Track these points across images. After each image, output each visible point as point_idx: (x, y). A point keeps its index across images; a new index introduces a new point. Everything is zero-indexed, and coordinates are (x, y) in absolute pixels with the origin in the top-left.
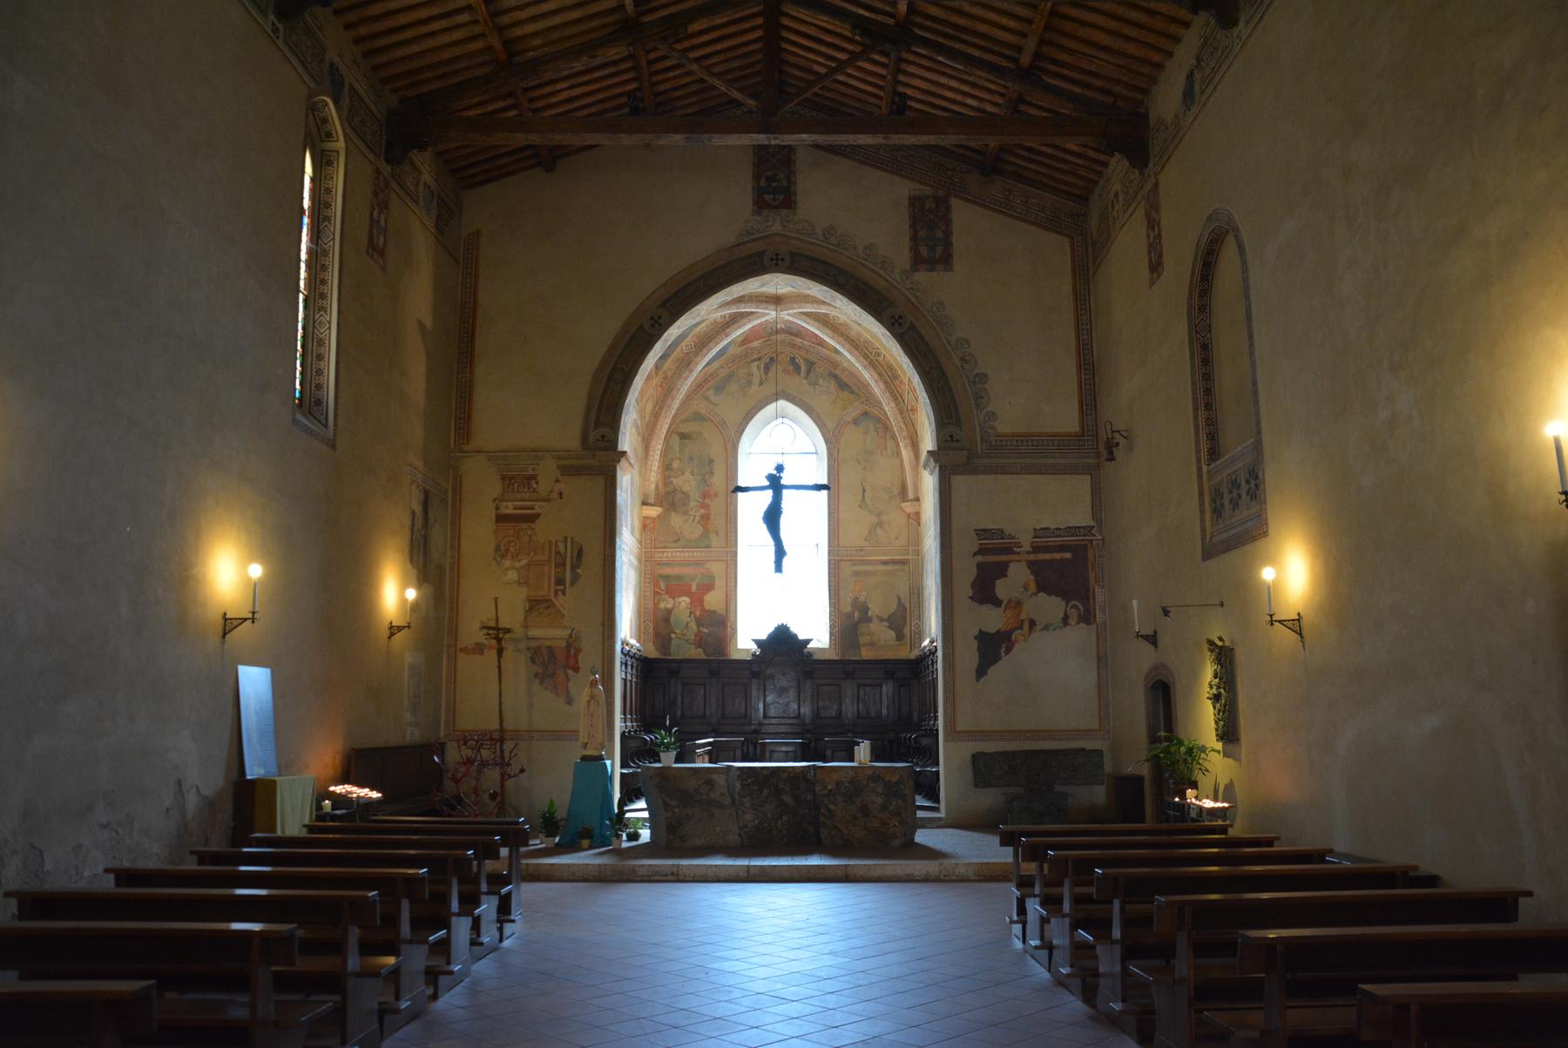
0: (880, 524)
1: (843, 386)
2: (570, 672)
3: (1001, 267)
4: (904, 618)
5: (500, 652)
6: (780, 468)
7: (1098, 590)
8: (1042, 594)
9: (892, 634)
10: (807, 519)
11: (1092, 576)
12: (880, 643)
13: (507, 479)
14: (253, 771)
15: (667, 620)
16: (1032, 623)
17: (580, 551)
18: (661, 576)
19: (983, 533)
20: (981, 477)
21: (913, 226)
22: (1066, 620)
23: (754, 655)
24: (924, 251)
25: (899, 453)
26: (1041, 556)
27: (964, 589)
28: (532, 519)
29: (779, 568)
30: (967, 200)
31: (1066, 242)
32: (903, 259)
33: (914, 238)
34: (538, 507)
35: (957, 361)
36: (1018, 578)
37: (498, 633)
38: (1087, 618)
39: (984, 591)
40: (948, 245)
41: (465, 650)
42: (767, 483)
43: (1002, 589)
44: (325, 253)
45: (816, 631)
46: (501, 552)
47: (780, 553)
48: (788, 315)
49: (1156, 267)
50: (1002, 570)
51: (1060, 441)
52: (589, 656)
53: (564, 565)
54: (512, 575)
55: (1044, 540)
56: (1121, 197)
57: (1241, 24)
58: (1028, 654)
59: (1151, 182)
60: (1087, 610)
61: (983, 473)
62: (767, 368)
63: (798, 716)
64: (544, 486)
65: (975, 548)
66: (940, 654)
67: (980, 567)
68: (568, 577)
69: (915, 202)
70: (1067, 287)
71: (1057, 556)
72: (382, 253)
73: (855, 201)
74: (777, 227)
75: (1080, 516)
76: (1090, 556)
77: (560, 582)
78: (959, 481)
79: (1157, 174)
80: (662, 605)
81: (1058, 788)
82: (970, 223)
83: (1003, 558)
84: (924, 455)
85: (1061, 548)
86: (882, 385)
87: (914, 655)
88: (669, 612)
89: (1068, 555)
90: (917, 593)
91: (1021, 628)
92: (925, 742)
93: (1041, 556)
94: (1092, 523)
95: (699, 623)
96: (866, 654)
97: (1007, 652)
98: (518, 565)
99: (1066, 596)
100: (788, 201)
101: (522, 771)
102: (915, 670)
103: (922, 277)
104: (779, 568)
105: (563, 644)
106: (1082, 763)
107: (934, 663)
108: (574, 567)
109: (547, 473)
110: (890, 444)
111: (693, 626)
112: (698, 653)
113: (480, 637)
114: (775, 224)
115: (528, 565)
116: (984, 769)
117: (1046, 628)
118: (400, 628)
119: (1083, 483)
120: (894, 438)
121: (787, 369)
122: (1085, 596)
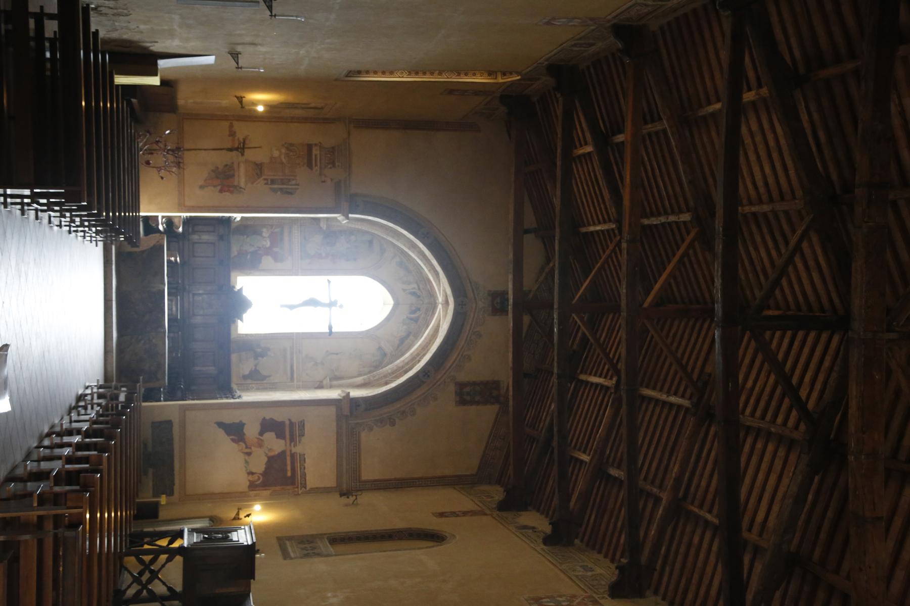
0: (316, 364)
1: (402, 341)
2: (219, 188)
4: (257, 379)
5: (231, 150)
6: (341, 306)
7: (268, 492)
8: (266, 459)
9: (247, 372)
10: (311, 322)
11: (278, 488)
12: (241, 366)
13: (333, 150)
14: (162, 63)
16: (249, 454)
17: (290, 193)
19: (302, 425)
20: (335, 424)
21: (482, 383)
22: (251, 473)
23: (234, 287)
24: (467, 389)
25: (360, 375)
26: (288, 458)
27: (269, 414)
28: (310, 165)
29: (282, 306)
30: (497, 415)
32: (463, 377)
33: (475, 384)
36: (276, 445)
37: (241, 148)
38: (252, 486)
39: (268, 426)
40: (472, 403)
41: (231, 126)
42: (333, 300)
43: (270, 436)
45: (247, 326)
46: (290, 147)
47: (292, 307)
49: (442, 515)
50: (280, 435)
51: (356, 470)
52: (228, 198)
53: (283, 184)
54: (276, 153)
55: (297, 460)
56: (589, 574)
57: (544, 547)
58: (226, 447)
59: (488, 512)
60: (257, 486)
61: (337, 424)
62: (413, 294)
63: (194, 315)
65: (293, 420)
66: (232, 401)
67: (282, 425)
68: (276, 186)
69: (496, 384)
70: (447, 472)
71: (289, 468)
72: (548, 23)
73: (493, 359)
75: (312, 481)
76: (288, 487)
77: (273, 182)
78: (333, 410)
79: (492, 515)
81: (151, 471)
82: (484, 416)
83: (288, 436)
84: (348, 391)
85: (293, 470)
86: (401, 365)
87: (234, 386)
88: (260, 234)
89: (289, 474)
90: (274, 387)
91: (247, 447)
92: (179, 394)
93: (288, 458)
94: (308, 488)
96: (234, 357)
98: (283, 157)
99: (265, 474)
101: (162, 178)
102: (226, 390)
103: (452, 388)
104: (282, 306)
105: (236, 183)
106: (165, 485)
107: (227, 398)
108: (281, 189)
110: (367, 370)
111: (252, 249)
112: (235, 250)
113: (240, 136)
115: (282, 163)
117: (247, 462)
118: (241, 102)
119: (331, 482)
120: (370, 372)
121: (415, 307)
122: (265, 485)
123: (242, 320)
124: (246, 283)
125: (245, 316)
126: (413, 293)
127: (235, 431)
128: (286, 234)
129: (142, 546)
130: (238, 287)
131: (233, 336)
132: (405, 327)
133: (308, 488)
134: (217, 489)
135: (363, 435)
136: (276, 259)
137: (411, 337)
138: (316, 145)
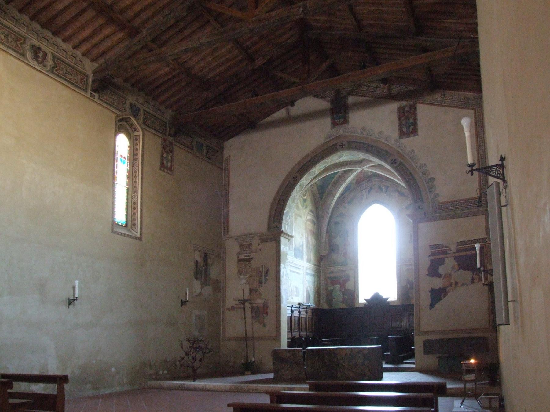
2: (265, 315)
3: (444, 126)
13: (242, 246)
15: (331, 294)
18: (328, 278)
21: (399, 119)
22: (473, 281)
23: (365, 304)
24: (404, 130)
28: (250, 260)
31: (473, 111)
33: (400, 125)
34: (252, 255)
35: (421, 175)
36: (450, 263)
40: (415, 124)
41: (228, 309)
43: (442, 270)
44: (136, 172)
45: (391, 293)
48: (366, 168)
50: (441, 262)
51: (469, 202)
54: (244, 281)
64: (255, 247)
74: (341, 132)
77: (260, 282)
80: (329, 288)
82: (425, 112)
83: (442, 256)
91: (451, 285)
94: (486, 236)
95: (344, 294)
97: (444, 297)
98: (245, 277)
100: (346, 121)
108: (265, 276)
109: (255, 243)
111: (341, 295)
112: (344, 306)
114: (340, 131)
115: (249, 277)
116: (429, 347)
117: (463, 285)
121: (368, 187)
123: (388, 299)
124: (364, 296)
125: (384, 296)
126: (369, 192)
127: (437, 295)
128: (331, 275)
129: (380, 378)
130: (365, 302)
131: (399, 304)
132: (392, 193)
133: (486, 236)
134: (485, 306)
135: (442, 199)
136: (347, 280)
137: (399, 189)
138: (238, 257)
